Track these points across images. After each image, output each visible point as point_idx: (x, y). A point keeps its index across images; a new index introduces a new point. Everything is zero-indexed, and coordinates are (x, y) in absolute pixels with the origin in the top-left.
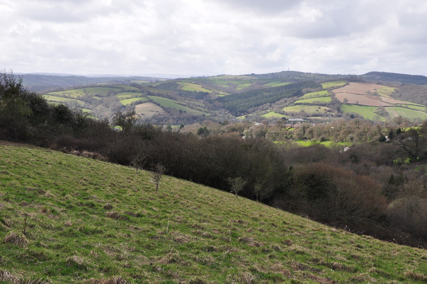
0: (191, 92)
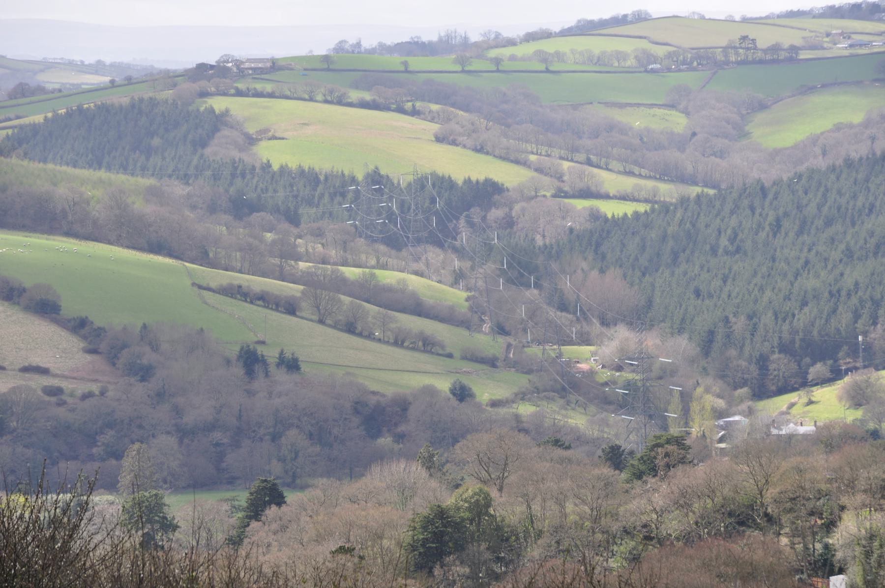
0: (338, 187)
